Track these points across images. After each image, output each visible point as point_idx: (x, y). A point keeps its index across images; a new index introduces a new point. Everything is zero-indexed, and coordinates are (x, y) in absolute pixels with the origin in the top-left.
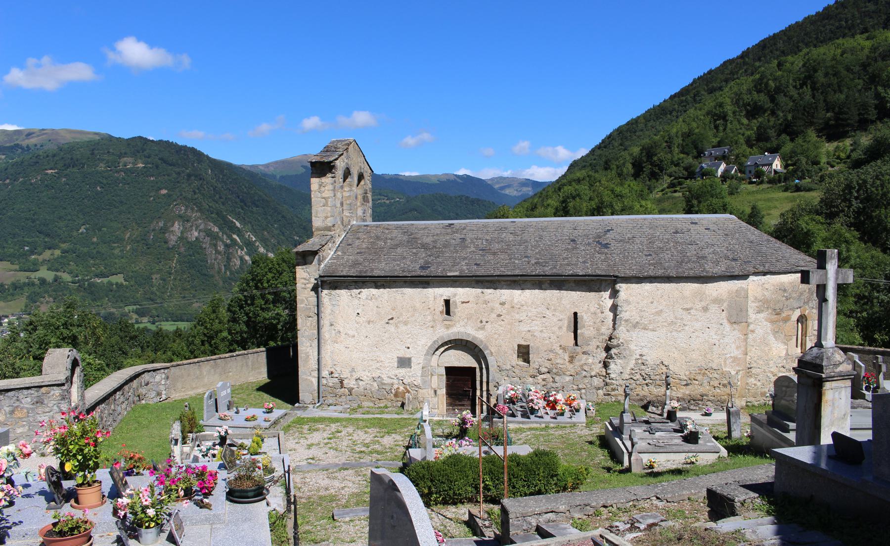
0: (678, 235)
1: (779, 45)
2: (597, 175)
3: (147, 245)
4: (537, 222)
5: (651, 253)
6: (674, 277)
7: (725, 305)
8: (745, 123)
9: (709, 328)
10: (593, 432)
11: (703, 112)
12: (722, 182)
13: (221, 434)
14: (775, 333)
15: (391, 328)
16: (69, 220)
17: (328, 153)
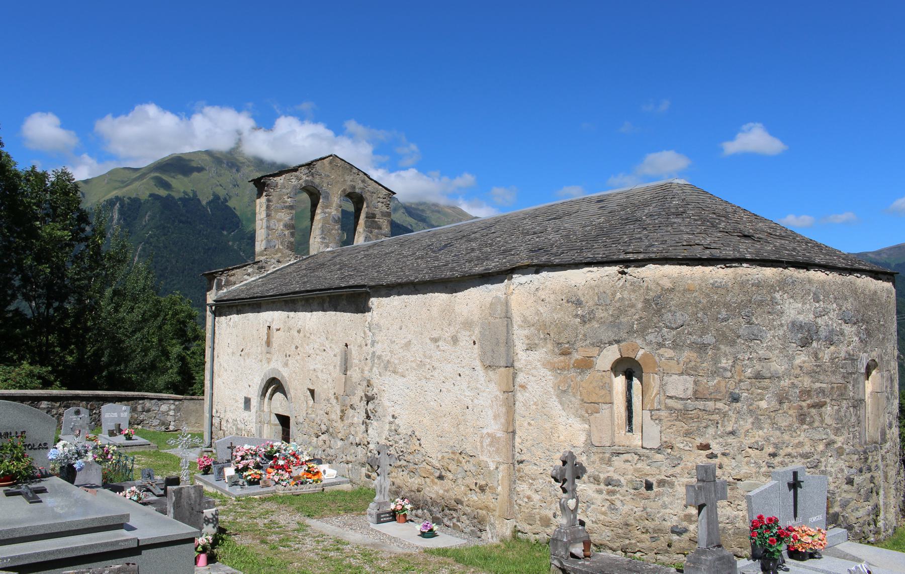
7: (477, 331)
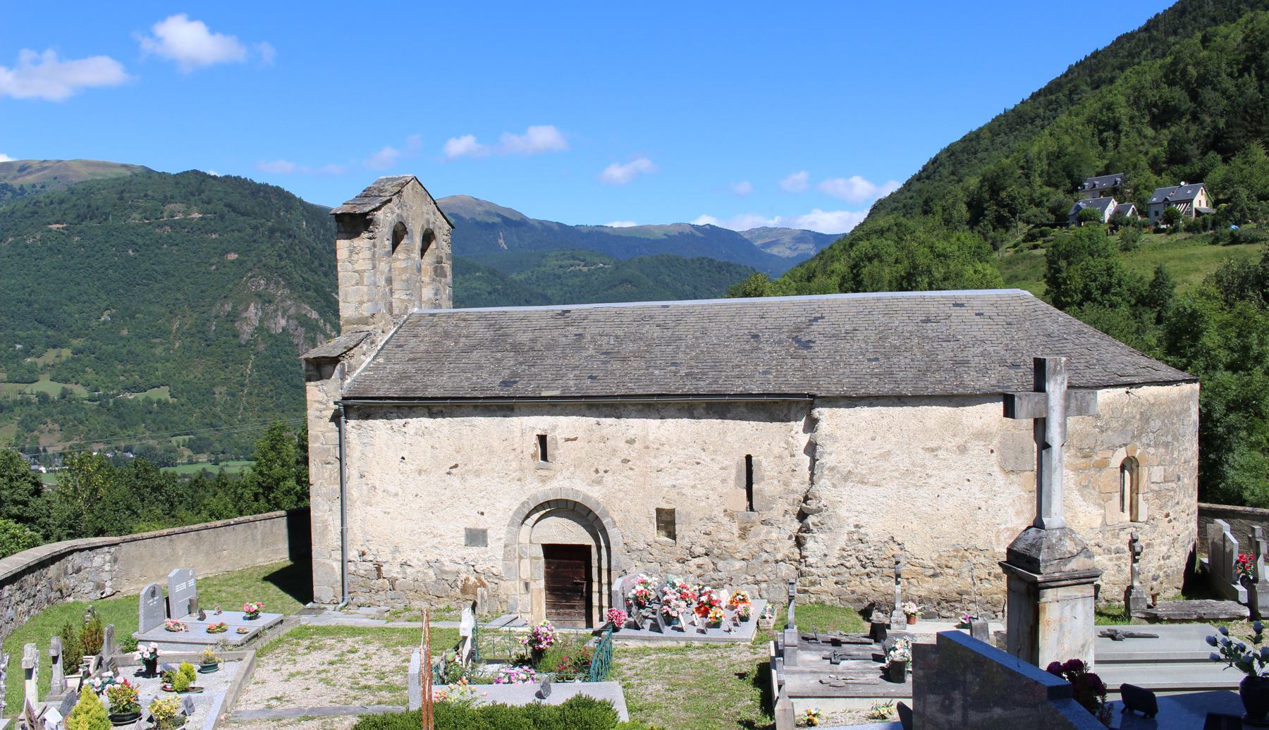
0: (929, 324)
1: (1206, 8)
2: (911, 223)
3: (206, 341)
4: (703, 306)
5: (879, 356)
6: (907, 396)
7: (996, 442)
8: (1149, 135)
9: (969, 480)
10: (756, 656)
11: (1082, 119)
12: (1111, 231)
13: (144, 656)
14: (1082, 488)
15: (455, 481)
16: (85, 302)
17: (367, 200)
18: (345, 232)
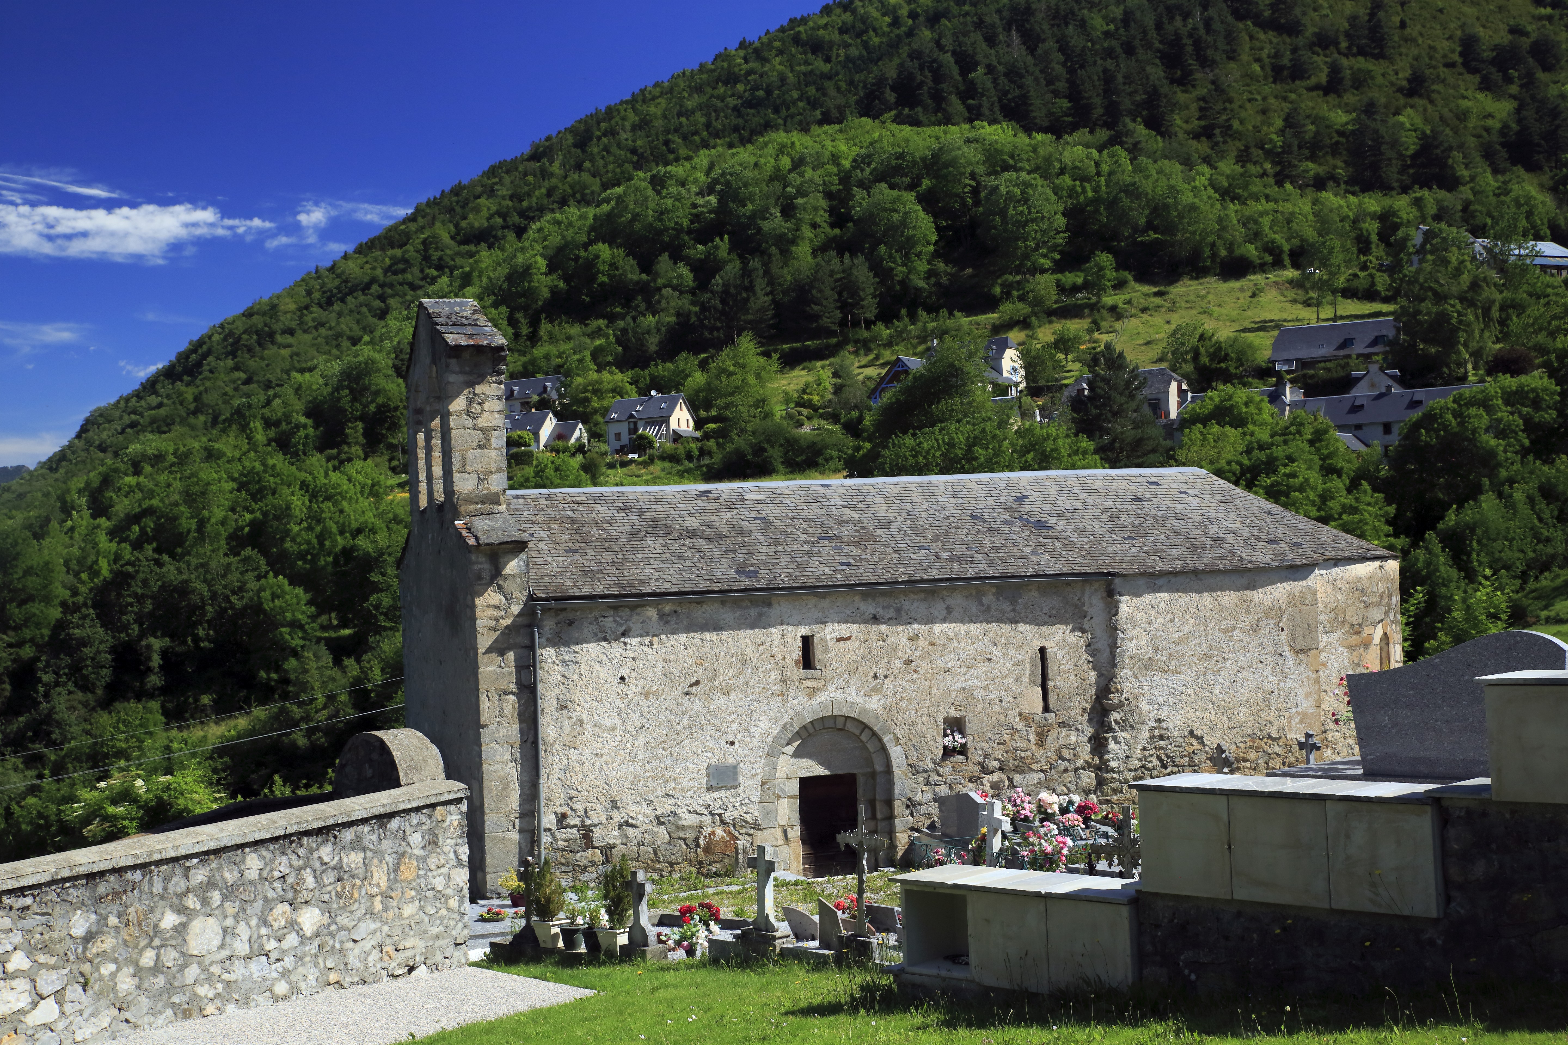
18: (461, 372)
